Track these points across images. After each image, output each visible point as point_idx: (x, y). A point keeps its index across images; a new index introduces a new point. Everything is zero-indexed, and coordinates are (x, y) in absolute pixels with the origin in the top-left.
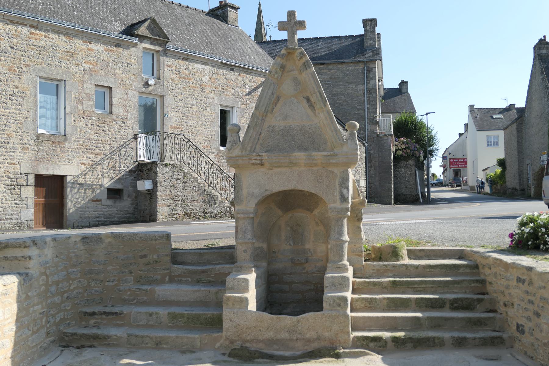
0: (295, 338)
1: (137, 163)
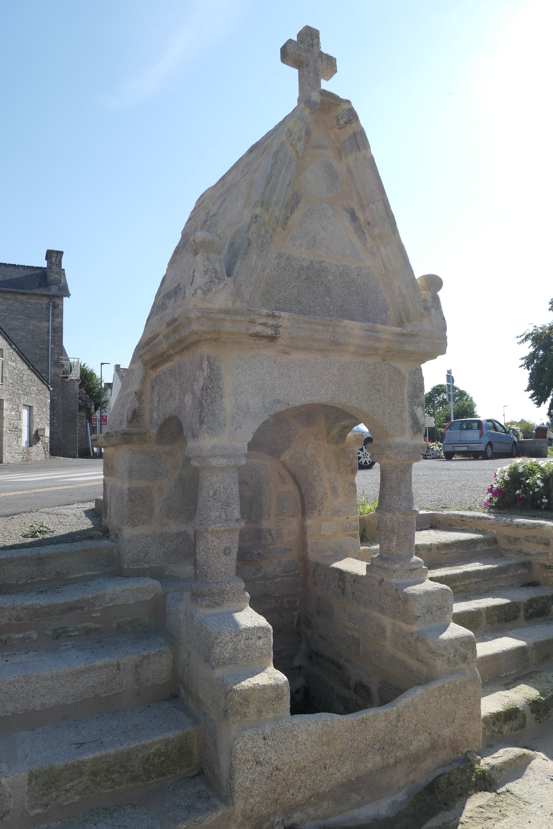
0: (391, 761)
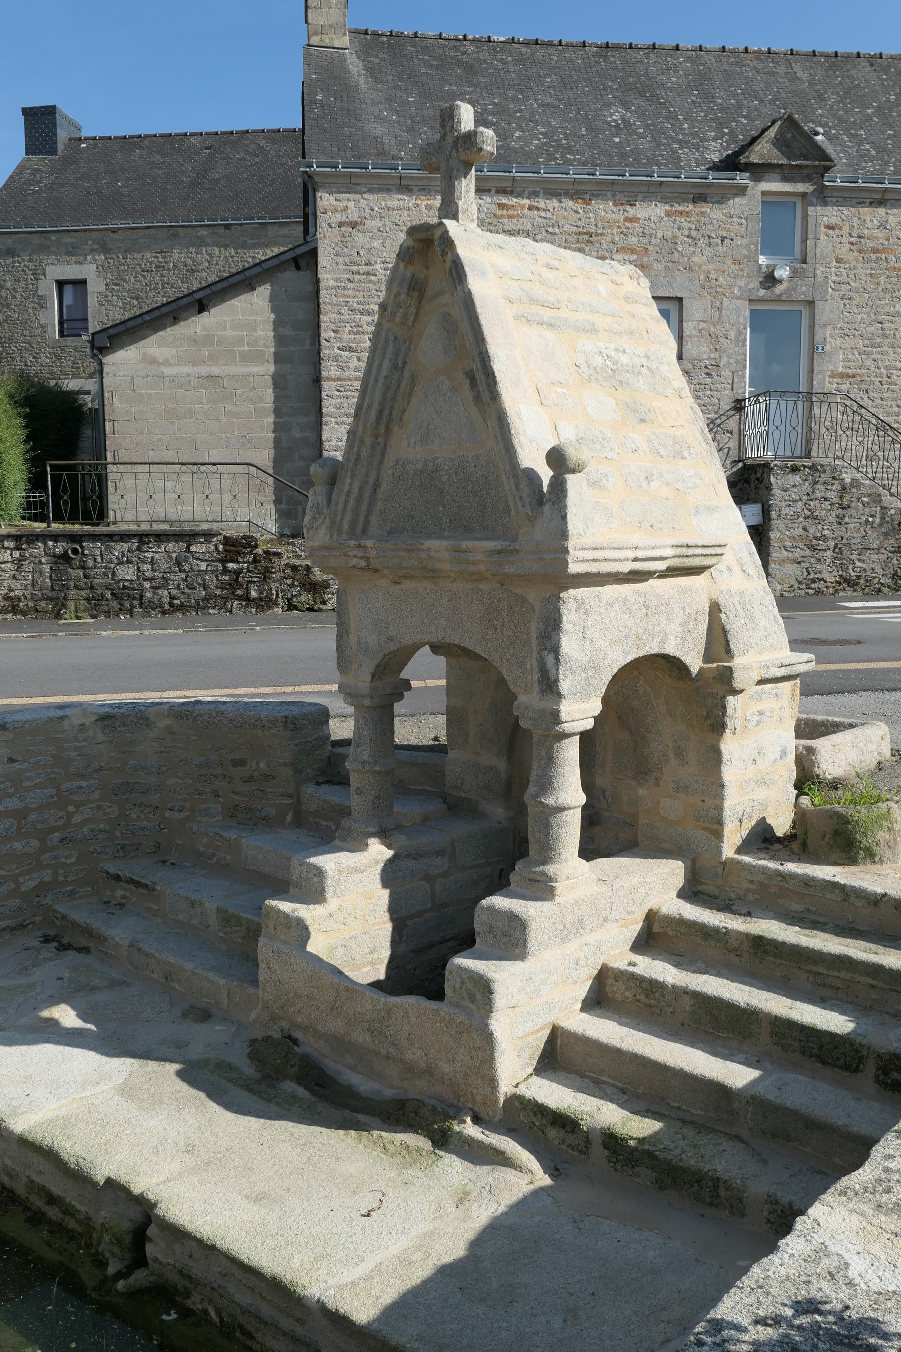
1: (741, 464)
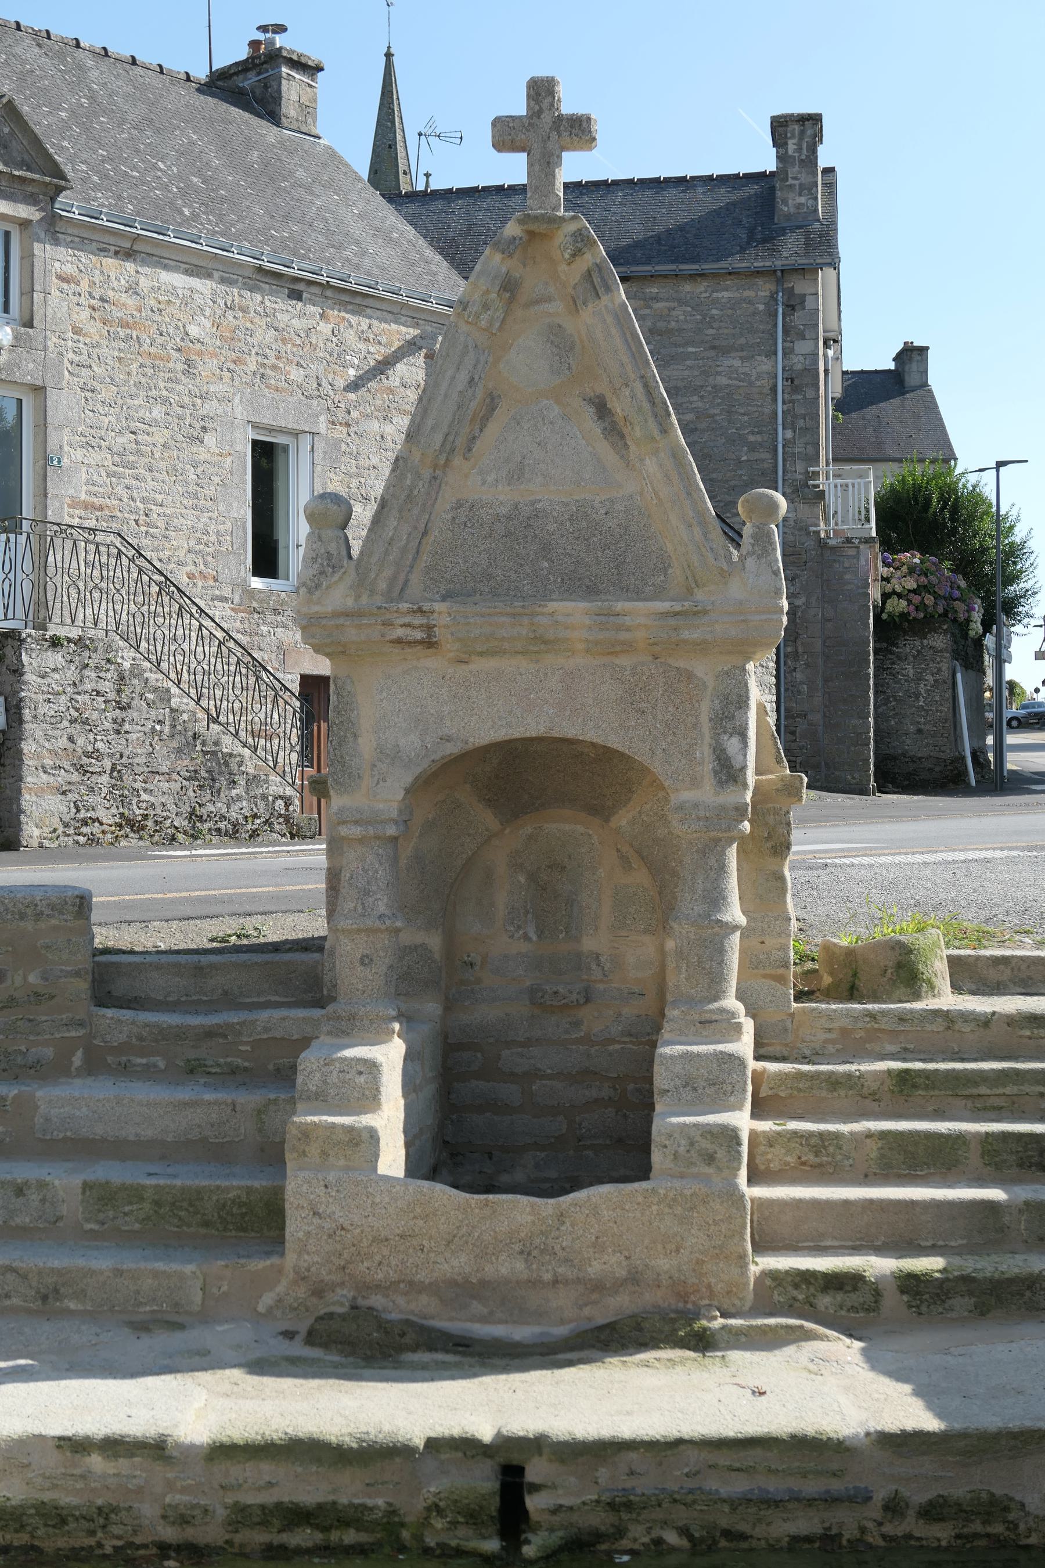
0: (547, 1277)
